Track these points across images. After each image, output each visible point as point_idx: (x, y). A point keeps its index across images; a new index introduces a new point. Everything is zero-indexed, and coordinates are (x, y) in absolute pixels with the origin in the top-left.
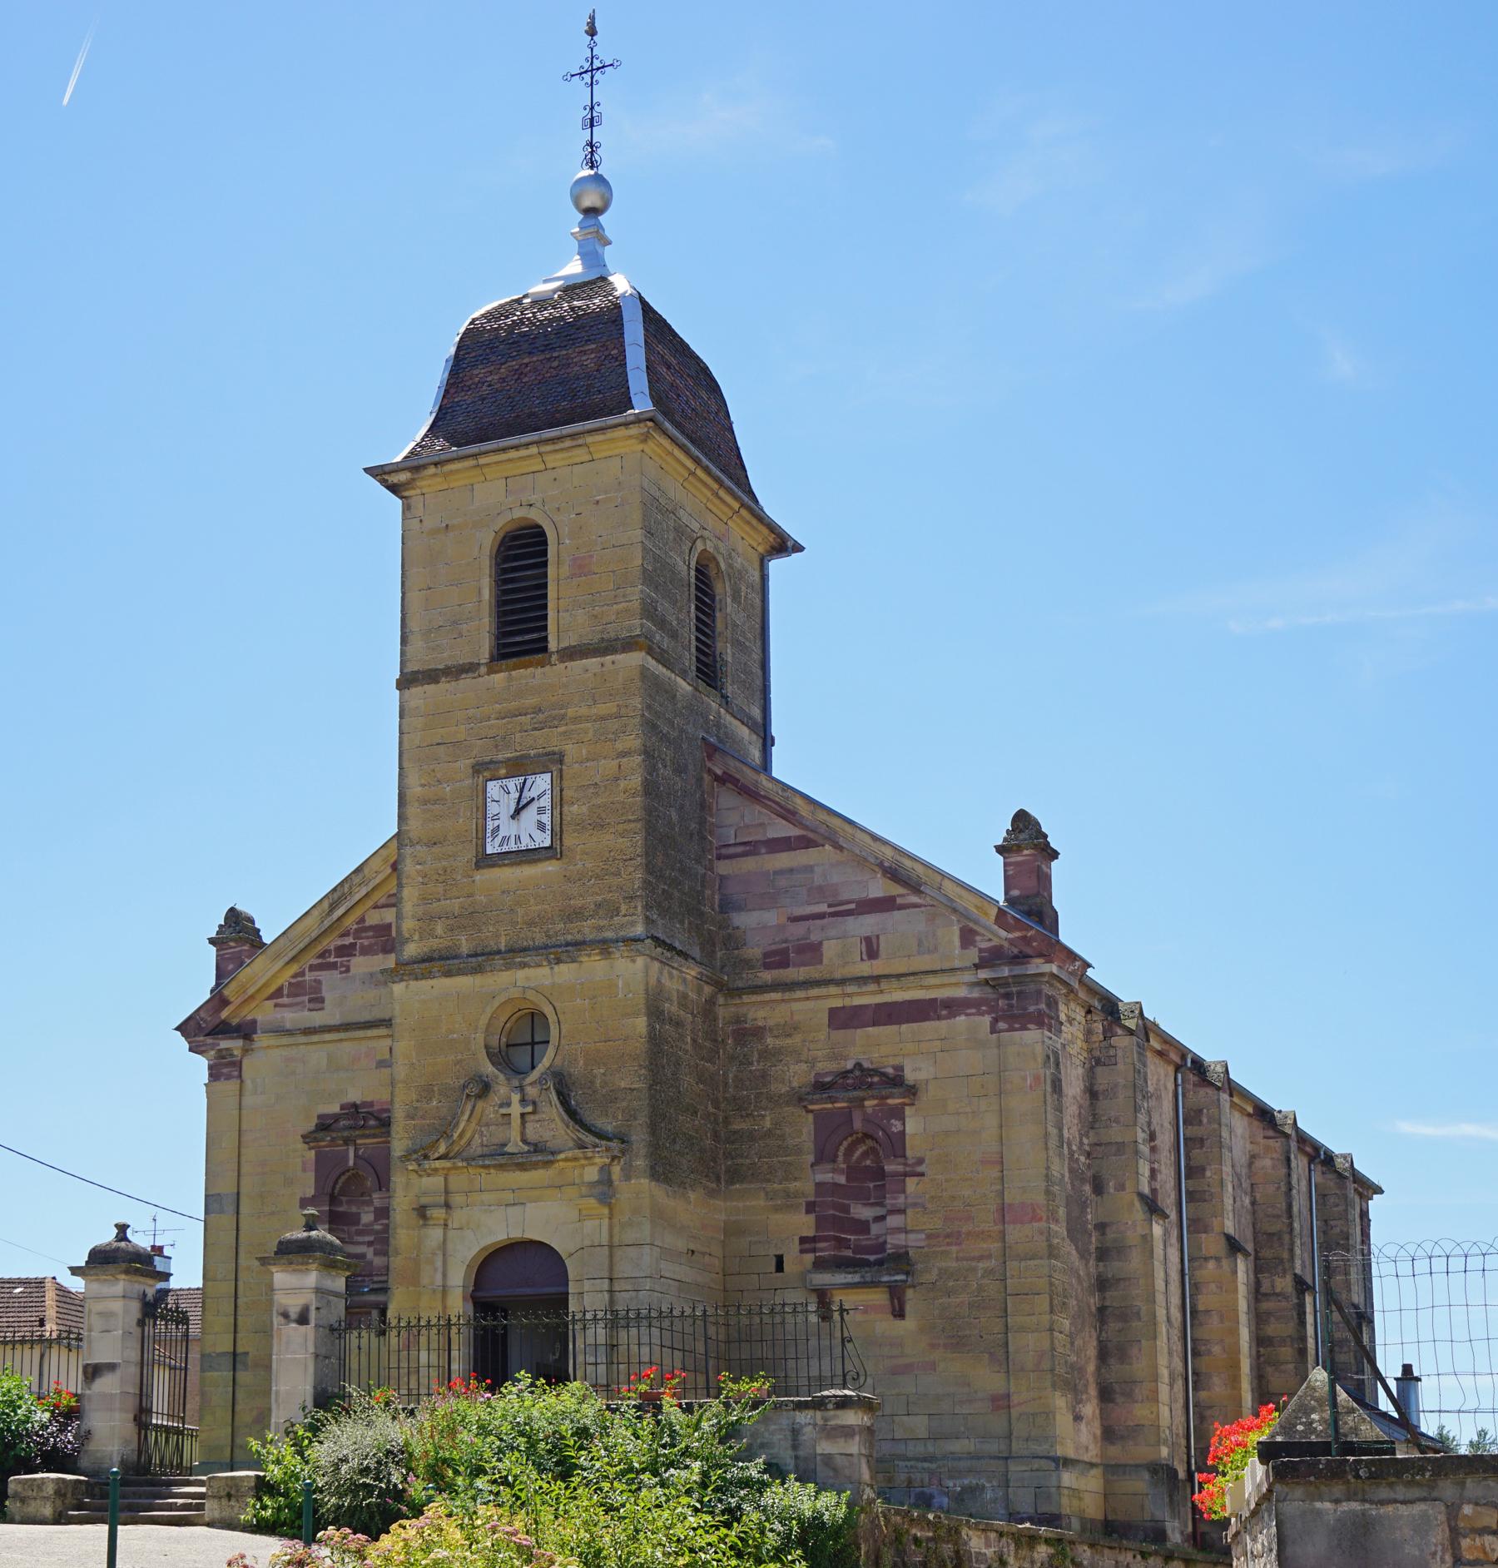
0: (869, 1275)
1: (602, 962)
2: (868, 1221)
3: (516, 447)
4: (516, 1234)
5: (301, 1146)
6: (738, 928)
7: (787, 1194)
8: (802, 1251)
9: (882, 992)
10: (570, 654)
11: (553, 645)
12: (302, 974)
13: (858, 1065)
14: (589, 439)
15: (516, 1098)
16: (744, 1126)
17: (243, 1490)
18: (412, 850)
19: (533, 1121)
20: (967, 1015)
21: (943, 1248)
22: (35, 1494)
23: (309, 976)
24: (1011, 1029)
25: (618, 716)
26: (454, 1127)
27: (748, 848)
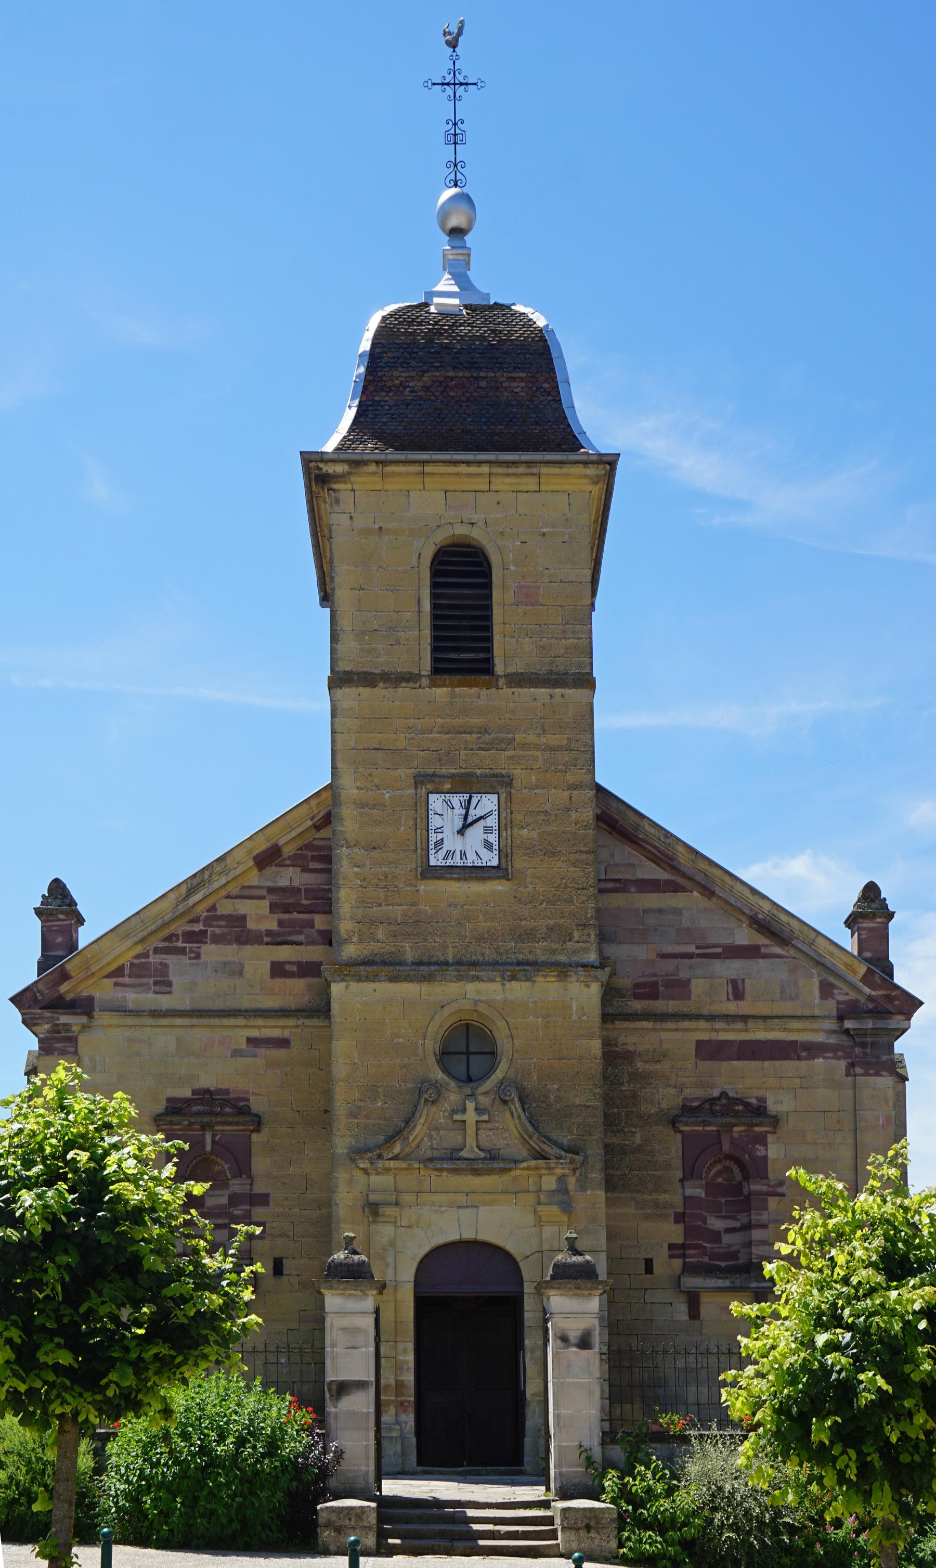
0: (738, 1281)
1: (556, 984)
2: (719, 1232)
3: (468, 463)
4: (468, 1235)
6: (608, 958)
7: (657, 1205)
8: (671, 1257)
9: (746, 1031)
10: (518, 680)
11: (499, 669)
12: (146, 955)
13: (724, 1094)
14: (544, 470)
15: (471, 1106)
17: (604, 1522)
18: (349, 851)
19: (485, 1129)
20: (824, 1058)
22: (353, 1523)
24: (866, 1074)
27: (618, 885)
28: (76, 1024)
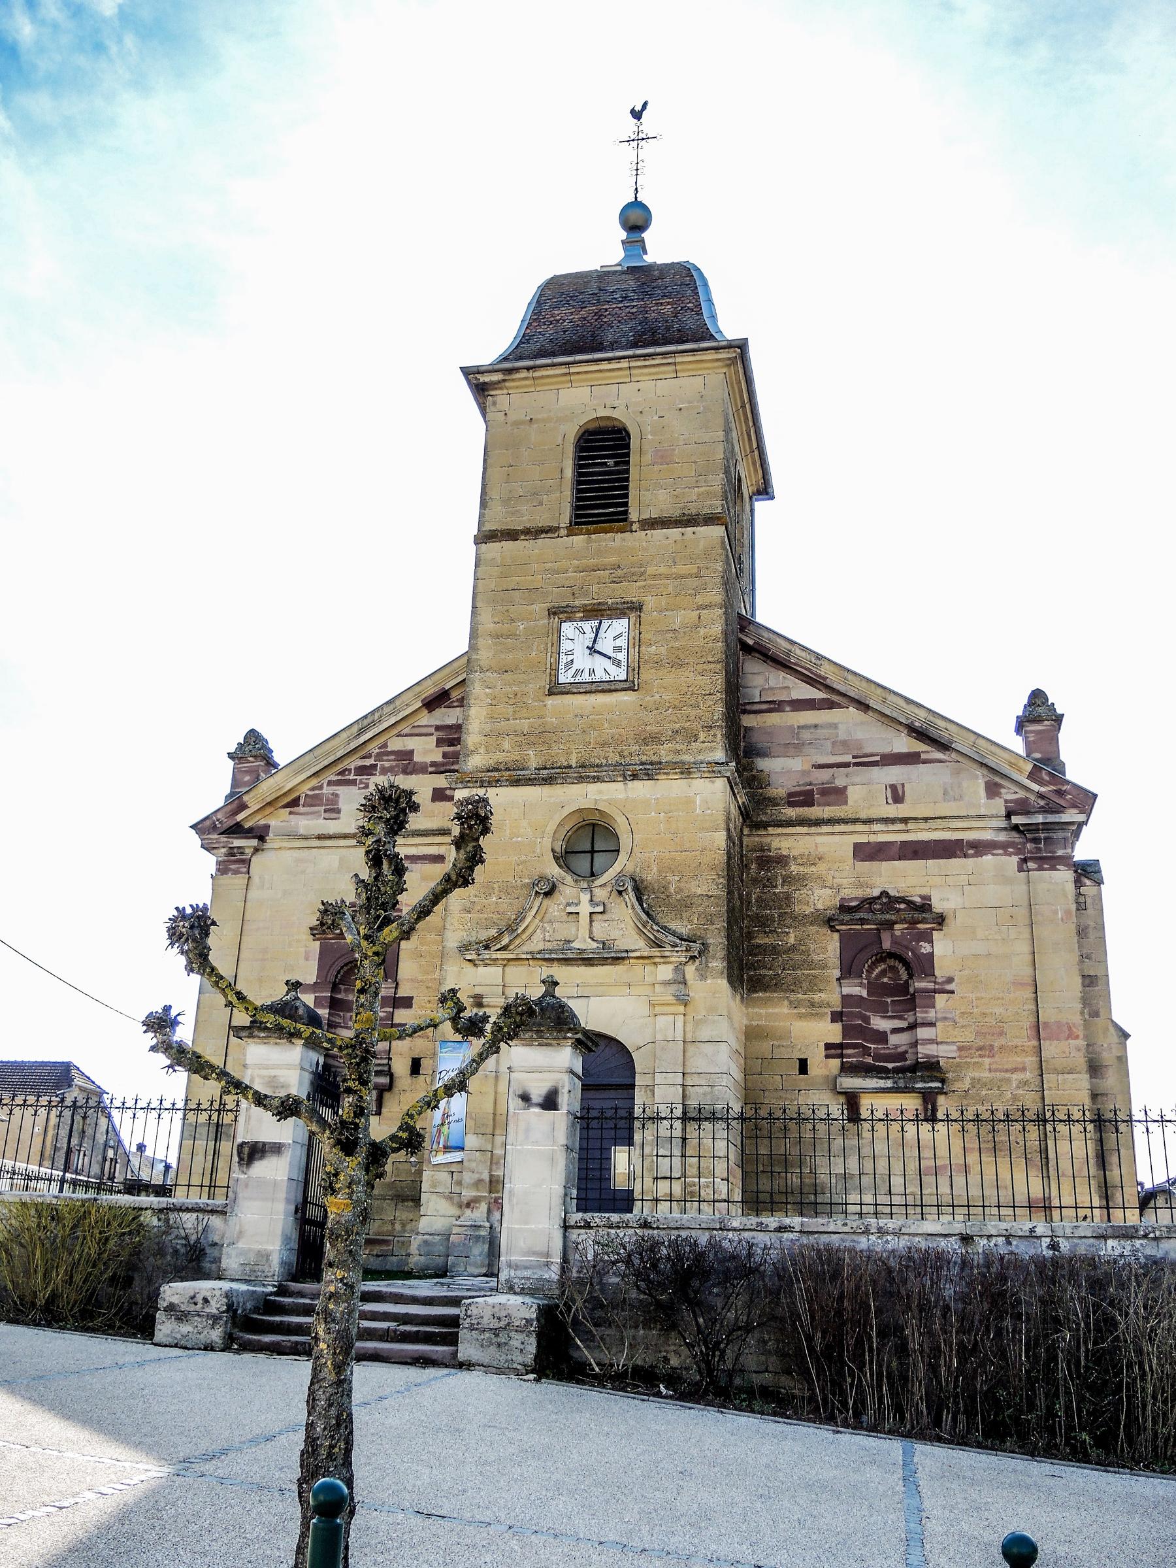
3: (609, 360)
5: (306, 936)
6: (762, 771)
7: (812, 1004)
8: (827, 1057)
11: (633, 515)
13: (884, 893)
15: (585, 897)
16: (767, 941)
20: (993, 855)
21: (976, 1060)
23: (326, 790)
24: (1040, 869)
25: (698, 575)
26: (521, 921)
28: (248, 847)
